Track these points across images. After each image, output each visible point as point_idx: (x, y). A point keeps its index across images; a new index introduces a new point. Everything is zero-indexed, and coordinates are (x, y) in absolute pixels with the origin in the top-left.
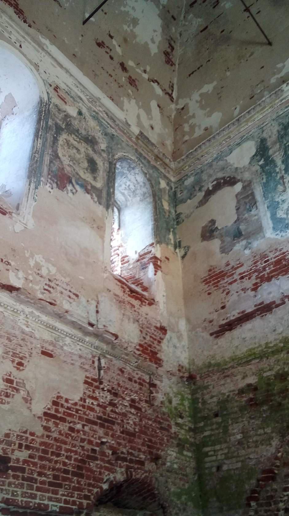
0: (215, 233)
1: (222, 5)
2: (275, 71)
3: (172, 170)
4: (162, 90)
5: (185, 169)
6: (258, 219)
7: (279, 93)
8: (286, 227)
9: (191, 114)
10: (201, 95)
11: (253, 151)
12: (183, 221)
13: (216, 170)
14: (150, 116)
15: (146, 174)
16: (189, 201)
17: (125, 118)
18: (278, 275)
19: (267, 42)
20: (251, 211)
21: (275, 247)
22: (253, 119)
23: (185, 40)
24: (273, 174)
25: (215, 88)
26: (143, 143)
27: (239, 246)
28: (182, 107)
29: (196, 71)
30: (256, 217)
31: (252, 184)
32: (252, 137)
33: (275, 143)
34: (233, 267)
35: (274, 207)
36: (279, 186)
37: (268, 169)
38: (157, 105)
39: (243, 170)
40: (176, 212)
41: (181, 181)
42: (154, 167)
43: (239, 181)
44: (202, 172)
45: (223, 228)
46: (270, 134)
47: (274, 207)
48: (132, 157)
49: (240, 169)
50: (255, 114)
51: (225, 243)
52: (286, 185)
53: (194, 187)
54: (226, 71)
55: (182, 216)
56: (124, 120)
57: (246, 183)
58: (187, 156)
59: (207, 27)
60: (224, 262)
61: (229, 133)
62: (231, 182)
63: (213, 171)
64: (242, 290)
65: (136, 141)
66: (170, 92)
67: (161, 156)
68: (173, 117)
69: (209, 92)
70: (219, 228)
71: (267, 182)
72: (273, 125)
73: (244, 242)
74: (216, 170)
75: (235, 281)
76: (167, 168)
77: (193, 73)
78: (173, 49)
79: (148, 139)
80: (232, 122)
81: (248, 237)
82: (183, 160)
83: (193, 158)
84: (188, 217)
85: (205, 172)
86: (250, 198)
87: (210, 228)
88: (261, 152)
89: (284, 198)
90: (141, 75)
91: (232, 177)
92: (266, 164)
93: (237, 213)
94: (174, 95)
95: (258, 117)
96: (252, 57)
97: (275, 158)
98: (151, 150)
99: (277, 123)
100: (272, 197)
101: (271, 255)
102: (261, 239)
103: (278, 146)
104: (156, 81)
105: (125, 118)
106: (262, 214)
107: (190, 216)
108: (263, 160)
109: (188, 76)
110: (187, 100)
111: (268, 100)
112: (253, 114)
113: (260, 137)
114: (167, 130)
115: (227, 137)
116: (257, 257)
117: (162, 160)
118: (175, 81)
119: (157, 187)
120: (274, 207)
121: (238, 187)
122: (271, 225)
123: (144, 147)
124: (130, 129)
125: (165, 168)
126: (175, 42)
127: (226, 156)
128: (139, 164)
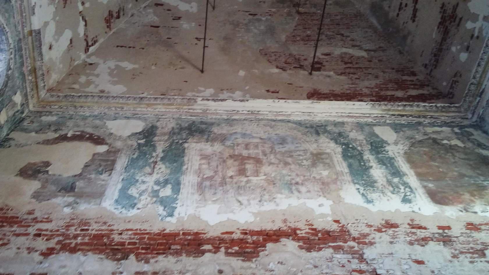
0: (40, 175)
1: (182, 22)
2: (196, 90)
3: (38, 97)
4: (85, 34)
5: (52, 107)
6: (106, 185)
7: (192, 101)
8: (131, 206)
9: (96, 72)
10: (117, 67)
11: (140, 130)
12: (9, 147)
13: (87, 125)
14: (56, 37)
15: (10, 69)
16: (33, 134)
17: (35, 3)
18: (89, 251)
19: (201, 68)
20: (101, 174)
21: (104, 220)
22: (155, 107)
23: (133, 22)
24: (147, 156)
25: (134, 69)
26: (32, 43)
27: (59, 200)
28: (91, 62)
29: (126, 47)
30: (103, 183)
31: (120, 153)
32: (145, 120)
33: (164, 134)
34: (36, 218)
35: (129, 182)
36: (147, 168)
37: (144, 150)
38: (70, 39)
39: (118, 138)
40: (8, 135)
41: (40, 114)
42: (23, 74)
43: (106, 144)
44: (71, 118)
45: (54, 175)
46: (164, 126)
47: (131, 183)
48: (10, 39)
49: (116, 136)
50: (159, 104)
51: (45, 190)
52: (155, 170)
53: (50, 126)
54: (153, 65)
55: (12, 143)
56: (33, 4)
57: (113, 150)
58: (66, 96)
59: (158, 27)
60: (29, 208)
61: (125, 104)
62: (98, 141)
63: (83, 124)
64: (28, 249)
65: (26, 34)
66: (90, 44)
67: (39, 73)
68: (76, 63)
69: (127, 69)
70: (50, 173)
71: (137, 158)
72: (171, 121)
73: (71, 199)
74: (87, 125)
75: (27, 234)
76: (35, 91)
77: (122, 47)
78: (118, 17)
79: (41, 45)
80: (135, 96)
81: (81, 196)
82: (58, 96)
83: (71, 102)
84: (18, 146)
85: (73, 120)
86: (109, 163)
87: (39, 168)
88: (147, 135)
89: (145, 179)
90: (78, 2)
91: (101, 137)
92: (146, 145)
93: (83, 169)
94: (91, 49)
95: (161, 109)
96: (181, 70)
97: (157, 145)
98: (34, 57)
99: (176, 122)
100: (134, 174)
101: (95, 226)
102: (94, 205)
103: (166, 137)
104: (86, 21)
105: (35, 3)
106: (111, 183)
107: (22, 146)
108: (144, 140)
109: (116, 46)
110: (101, 61)
111: (179, 101)
112: (158, 102)
113: (153, 124)
114: (61, 66)
115: (120, 106)
116: (75, 221)
117: (36, 78)
118: (101, 41)
119: (10, 93)
120: (129, 182)
121: (102, 149)
122: (116, 196)
123: (28, 48)
124: (32, 17)
125: (32, 90)
126: (124, 15)
127: (107, 120)
128: (11, 53)
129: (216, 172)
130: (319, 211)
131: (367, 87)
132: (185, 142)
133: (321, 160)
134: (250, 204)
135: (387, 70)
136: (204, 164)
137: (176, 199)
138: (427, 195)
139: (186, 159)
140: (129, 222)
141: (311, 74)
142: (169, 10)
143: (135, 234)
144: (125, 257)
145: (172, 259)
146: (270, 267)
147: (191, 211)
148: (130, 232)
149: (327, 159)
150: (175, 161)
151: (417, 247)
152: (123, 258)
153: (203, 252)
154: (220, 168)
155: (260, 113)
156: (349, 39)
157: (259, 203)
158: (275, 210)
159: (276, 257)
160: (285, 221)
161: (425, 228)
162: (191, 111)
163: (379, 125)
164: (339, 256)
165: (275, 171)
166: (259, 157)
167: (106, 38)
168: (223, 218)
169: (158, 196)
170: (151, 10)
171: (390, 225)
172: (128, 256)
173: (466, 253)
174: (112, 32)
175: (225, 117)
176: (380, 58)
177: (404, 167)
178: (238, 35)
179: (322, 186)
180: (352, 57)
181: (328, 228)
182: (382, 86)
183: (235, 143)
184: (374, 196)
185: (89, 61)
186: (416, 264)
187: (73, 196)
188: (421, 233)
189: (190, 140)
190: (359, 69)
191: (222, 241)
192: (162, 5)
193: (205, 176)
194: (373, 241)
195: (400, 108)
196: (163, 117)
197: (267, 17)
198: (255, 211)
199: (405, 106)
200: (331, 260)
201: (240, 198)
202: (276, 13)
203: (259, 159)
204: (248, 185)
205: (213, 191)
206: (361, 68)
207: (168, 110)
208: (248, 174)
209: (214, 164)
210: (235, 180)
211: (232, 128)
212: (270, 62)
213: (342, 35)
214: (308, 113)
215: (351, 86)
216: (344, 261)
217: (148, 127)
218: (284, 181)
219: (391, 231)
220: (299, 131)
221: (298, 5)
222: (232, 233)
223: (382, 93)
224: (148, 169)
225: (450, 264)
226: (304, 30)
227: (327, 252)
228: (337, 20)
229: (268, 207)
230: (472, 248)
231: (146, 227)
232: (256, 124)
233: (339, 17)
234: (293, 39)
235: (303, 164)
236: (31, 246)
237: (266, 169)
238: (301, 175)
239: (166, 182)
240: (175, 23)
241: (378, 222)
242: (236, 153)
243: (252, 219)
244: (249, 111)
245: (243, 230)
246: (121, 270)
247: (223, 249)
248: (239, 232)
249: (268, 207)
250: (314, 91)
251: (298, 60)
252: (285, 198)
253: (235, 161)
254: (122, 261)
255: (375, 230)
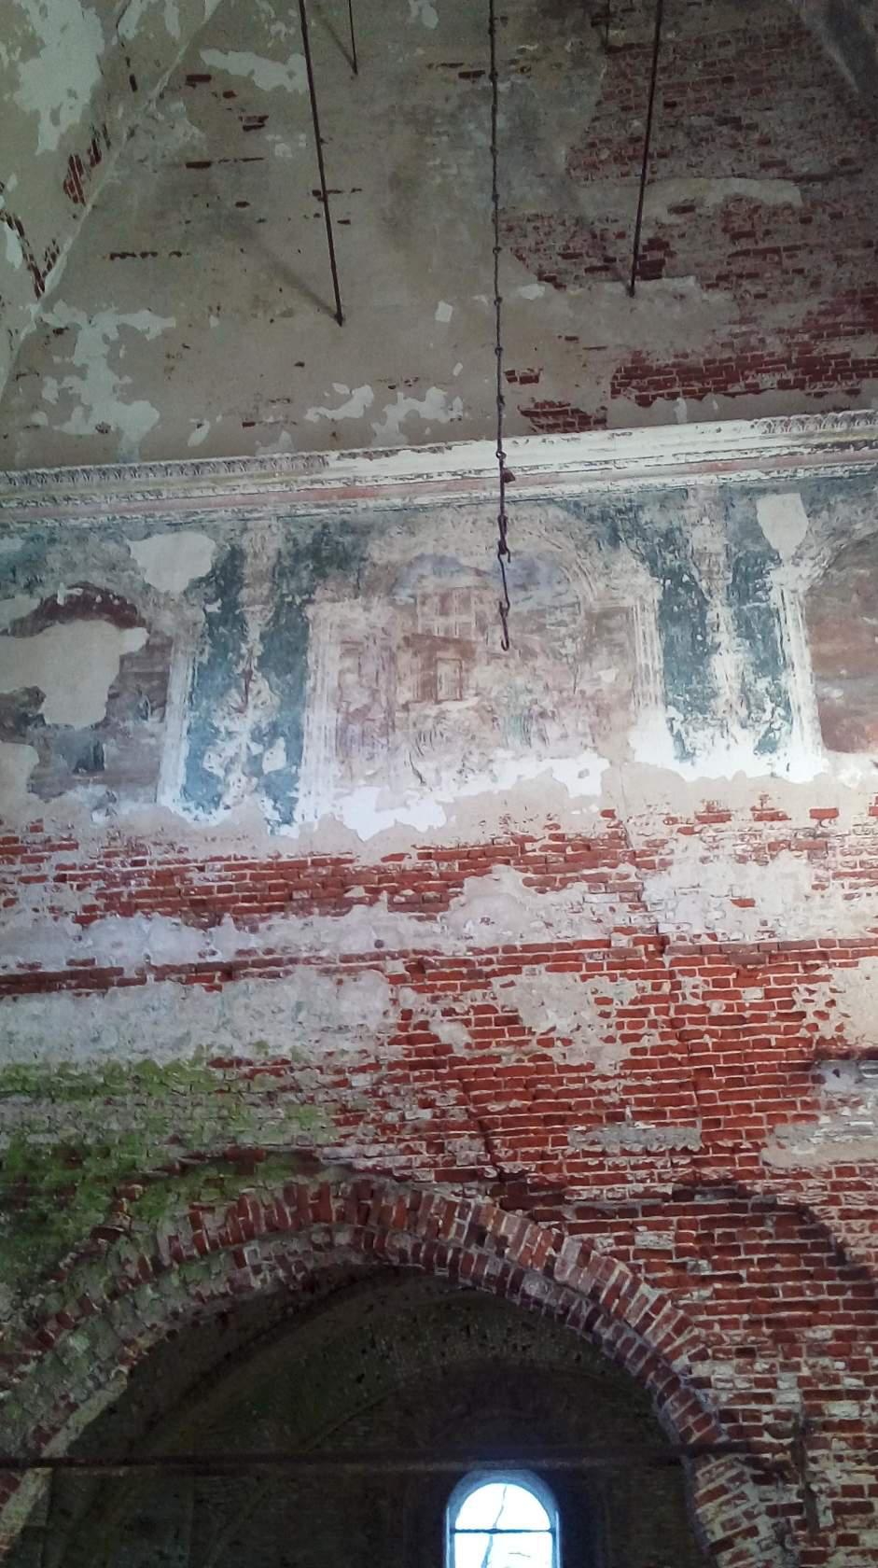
1: (269, 138)
4: (24, 256)
10: (122, 328)
21: (171, 838)
33: (259, 578)
34: (49, 840)
35: (204, 737)
43: (142, 623)
44: (52, 541)
50: (241, 478)
60: (29, 817)
62: (123, 615)
66: (42, 268)
68: (22, 336)
69: (148, 337)
72: (274, 529)
73: (100, 791)
75: (43, 879)
78: (97, 158)
93: (107, 705)
94: (49, 281)
97: (248, 617)
100: (208, 711)
102: (145, 802)
111: (285, 465)
120: (204, 737)
121: (135, 639)
129: (374, 693)
130: (578, 788)
131: (780, 331)
132: (310, 601)
133: (606, 636)
134: (439, 781)
135: (849, 252)
136: (349, 670)
137: (295, 778)
138: (817, 725)
139: (311, 657)
140: (213, 840)
141: (631, 291)
142: (229, 95)
143: (228, 868)
144: (216, 921)
145: (295, 921)
146: (466, 930)
147: (325, 809)
148: (218, 865)
149: (620, 629)
150: (289, 668)
151: (752, 867)
152: (212, 924)
153: (350, 904)
154: (383, 678)
155: (482, 475)
156: (756, 136)
157: (457, 776)
158: (488, 794)
159: (479, 908)
160: (505, 820)
161: (784, 818)
162: (317, 486)
163: (776, 491)
164: (600, 900)
165: (500, 681)
166: (468, 638)
167: (79, 229)
168: (386, 821)
169: (259, 773)
170: (179, 105)
171: (715, 815)
172: (220, 917)
173: (846, 875)
174: (89, 207)
175: (398, 502)
176: (838, 207)
177: (795, 642)
178: (431, 163)
179: (595, 719)
180: (757, 209)
181: (589, 833)
182: (822, 320)
183: (419, 592)
184: (698, 738)
185: (54, 321)
186: (736, 908)
187: (103, 782)
188: (772, 831)
189: (318, 595)
190: (769, 256)
191: (384, 876)
192: (206, 78)
193: (352, 709)
194: (668, 858)
195: (838, 429)
196: (256, 515)
197: (513, 77)
198: (449, 799)
199: (853, 419)
200: (577, 909)
201: (421, 768)
202: (538, 60)
203: (469, 642)
204: (439, 728)
205: (367, 749)
206: (776, 251)
207: (262, 489)
208: (441, 695)
209: (370, 668)
210: (413, 715)
211: (414, 540)
212: (521, 258)
213: (736, 123)
214: (601, 462)
215: (737, 329)
216: (603, 910)
217: (224, 556)
218: (515, 708)
219: (710, 832)
220: (571, 536)
221: (603, 18)
222: (400, 857)
223: (820, 349)
224: (235, 697)
225: (802, 905)
226: (623, 116)
227: (577, 890)
228: (726, 61)
229: (477, 785)
230: (862, 863)
231: (244, 850)
232: (471, 519)
233: (730, 52)
234: (587, 162)
235: (563, 651)
236: (55, 904)
237: (483, 674)
238: (555, 689)
239: (275, 730)
240: (251, 144)
241: (688, 810)
242: (420, 631)
243: (439, 820)
244: (455, 474)
245: (424, 848)
246: (212, 947)
247: (384, 896)
248: (414, 853)
249: (477, 785)
250: (633, 362)
251: (598, 239)
252: (513, 758)
253: (415, 654)
254: (212, 929)
255: (680, 831)
